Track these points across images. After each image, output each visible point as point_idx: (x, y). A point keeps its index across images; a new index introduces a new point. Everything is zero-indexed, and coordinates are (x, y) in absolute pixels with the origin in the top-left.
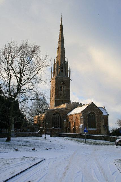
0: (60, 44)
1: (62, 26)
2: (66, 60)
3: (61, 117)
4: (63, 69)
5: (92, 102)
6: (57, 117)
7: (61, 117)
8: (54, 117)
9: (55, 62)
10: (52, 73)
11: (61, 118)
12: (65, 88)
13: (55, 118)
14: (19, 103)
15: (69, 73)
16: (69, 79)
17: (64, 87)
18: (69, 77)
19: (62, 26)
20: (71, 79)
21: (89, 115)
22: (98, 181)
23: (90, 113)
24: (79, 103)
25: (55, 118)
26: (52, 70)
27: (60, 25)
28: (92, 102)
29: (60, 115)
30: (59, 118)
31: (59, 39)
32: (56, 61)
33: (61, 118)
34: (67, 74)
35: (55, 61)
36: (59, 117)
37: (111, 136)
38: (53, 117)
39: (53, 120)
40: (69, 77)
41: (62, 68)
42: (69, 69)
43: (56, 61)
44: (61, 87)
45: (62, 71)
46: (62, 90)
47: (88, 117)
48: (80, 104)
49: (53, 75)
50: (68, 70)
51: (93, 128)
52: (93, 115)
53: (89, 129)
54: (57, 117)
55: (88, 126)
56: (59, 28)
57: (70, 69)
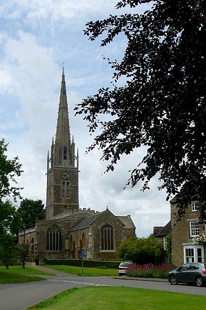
2: (71, 140)
4: (66, 154)
5: (107, 209)
7: (60, 233)
9: (53, 143)
15: (76, 161)
16: (76, 171)
17: (68, 183)
18: (76, 166)
21: (102, 230)
23: (105, 226)
26: (48, 156)
28: (107, 209)
30: (57, 234)
34: (72, 163)
36: (57, 231)
40: (76, 166)
41: (65, 152)
42: (76, 155)
43: (54, 140)
44: (64, 183)
45: (65, 158)
46: (65, 189)
47: (100, 233)
49: (50, 163)
50: (75, 156)
52: (109, 230)
55: (100, 247)
57: (78, 154)
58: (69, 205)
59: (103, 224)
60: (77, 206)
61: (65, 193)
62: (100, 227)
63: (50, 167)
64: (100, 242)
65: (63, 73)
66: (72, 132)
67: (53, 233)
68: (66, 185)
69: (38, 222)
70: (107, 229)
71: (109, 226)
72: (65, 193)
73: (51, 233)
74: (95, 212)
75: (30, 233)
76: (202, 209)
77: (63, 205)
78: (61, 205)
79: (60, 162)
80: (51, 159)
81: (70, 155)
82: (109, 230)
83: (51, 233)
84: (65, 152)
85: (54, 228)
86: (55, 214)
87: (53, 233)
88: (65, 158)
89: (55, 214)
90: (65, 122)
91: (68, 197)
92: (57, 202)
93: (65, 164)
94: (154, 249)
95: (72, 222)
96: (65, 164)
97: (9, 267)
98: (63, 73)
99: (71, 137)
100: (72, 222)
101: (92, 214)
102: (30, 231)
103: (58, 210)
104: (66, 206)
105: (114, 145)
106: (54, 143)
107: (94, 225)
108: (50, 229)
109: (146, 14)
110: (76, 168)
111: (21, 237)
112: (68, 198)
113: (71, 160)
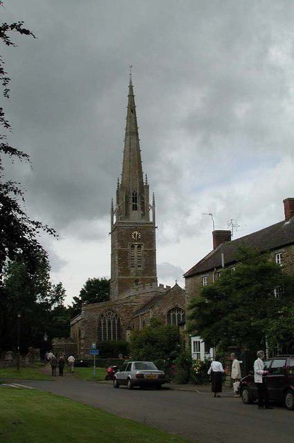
3: (119, 321)
4: (136, 202)
5: (177, 285)
7: (119, 321)
11: (119, 324)
12: (143, 248)
13: (105, 324)
14: (290, 244)
15: (151, 212)
17: (139, 246)
21: (169, 315)
23: (173, 310)
24: (163, 285)
25: (105, 324)
26: (112, 206)
27: (126, 104)
28: (177, 285)
29: (116, 316)
30: (114, 322)
32: (19, 216)
33: (119, 324)
34: (145, 215)
37: (143, 362)
39: (99, 328)
40: (151, 220)
41: (135, 200)
44: (133, 246)
47: (166, 320)
48: (165, 287)
49: (115, 217)
50: (149, 205)
57: (154, 202)
59: (170, 307)
60: (155, 280)
61: (136, 261)
62: (165, 312)
65: (131, 82)
66: (143, 169)
69: (85, 305)
71: (179, 310)
72: (136, 261)
73: (105, 322)
74: (165, 287)
75: (78, 321)
76: (284, 370)
79: (127, 214)
81: (143, 203)
83: (105, 322)
84: (135, 200)
86: (120, 292)
88: (135, 208)
89: (120, 292)
91: (140, 266)
92: (123, 275)
93: (135, 216)
94: (173, 358)
98: (131, 82)
99: (144, 175)
101: (161, 290)
103: (124, 286)
104: (137, 281)
105: (283, 328)
108: (102, 315)
112: (140, 268)
113: (143, 209)
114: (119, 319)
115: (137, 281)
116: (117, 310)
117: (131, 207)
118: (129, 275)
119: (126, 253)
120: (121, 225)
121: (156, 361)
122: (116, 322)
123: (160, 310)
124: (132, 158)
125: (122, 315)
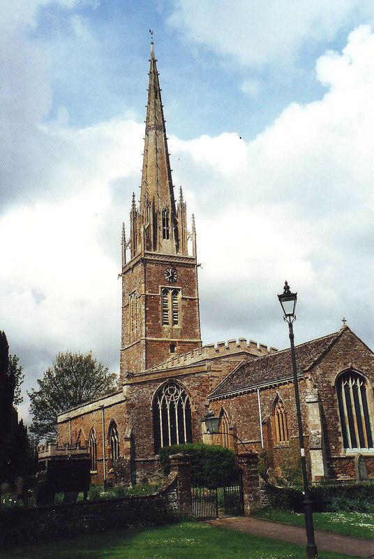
0: (152, 139)
1: (154, 74)
3: (188, 406)
6: (172, 405)
7: (188, 406)
8: (160, 403)
10: (124, 245)
12: (180, 295)
19: (154, 74)
20: (198, 263)
22: (24, 412)
30: (180, 406)
31: (148, 118)
35: (134, 201)
36: (180, 401)
38: (155, 406)
42: (189, 228)
43: (137, 199)
49: (128, 252)
51: (363, 446)
52: (355, 387)
53: (350, 452)
54: (172, 405)
55: (341, 439)
56: (146, 81)
57: (194, 229)
58: (179, 342)
62: (333, 379)
63: (128, 259)
64: (339, 424)
67: (168, 404)
68: (169, 297)
70: (351, 386)
73: (164, 405)
74: (268, 349)
75: (102, 408)
77: (166, 342)
78: (162, 342)
80: (131, 241)
81: (176, 231)
82: (355, 387)
83: (164, 405)
84: (165, 222)
85: (172, 391)
87: (168, 404)
88: (166, 235)
90: (162, 158)
95: (214, 374)
96: (167, 247)
97: (121, 278)
100: (214, 374)
102: (102, 403)
104: (173, 346)
106: (138, 205)
107: (318, 372)
109: (140, 248)
110: (191, 259)
111: (65, 425)
114: (188, 401)
115: (173, 346)
116: (185, 383)
117: (160, 233)
118: (160, 337)
119: (156, 299)
120: (148, 257)
121: (356, 460)
122: (168, 407)
123: (324, 374)
124: (159, 161)
125: (194, 393)
